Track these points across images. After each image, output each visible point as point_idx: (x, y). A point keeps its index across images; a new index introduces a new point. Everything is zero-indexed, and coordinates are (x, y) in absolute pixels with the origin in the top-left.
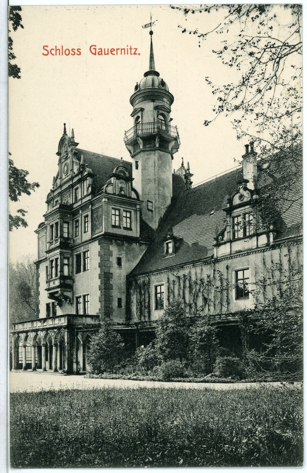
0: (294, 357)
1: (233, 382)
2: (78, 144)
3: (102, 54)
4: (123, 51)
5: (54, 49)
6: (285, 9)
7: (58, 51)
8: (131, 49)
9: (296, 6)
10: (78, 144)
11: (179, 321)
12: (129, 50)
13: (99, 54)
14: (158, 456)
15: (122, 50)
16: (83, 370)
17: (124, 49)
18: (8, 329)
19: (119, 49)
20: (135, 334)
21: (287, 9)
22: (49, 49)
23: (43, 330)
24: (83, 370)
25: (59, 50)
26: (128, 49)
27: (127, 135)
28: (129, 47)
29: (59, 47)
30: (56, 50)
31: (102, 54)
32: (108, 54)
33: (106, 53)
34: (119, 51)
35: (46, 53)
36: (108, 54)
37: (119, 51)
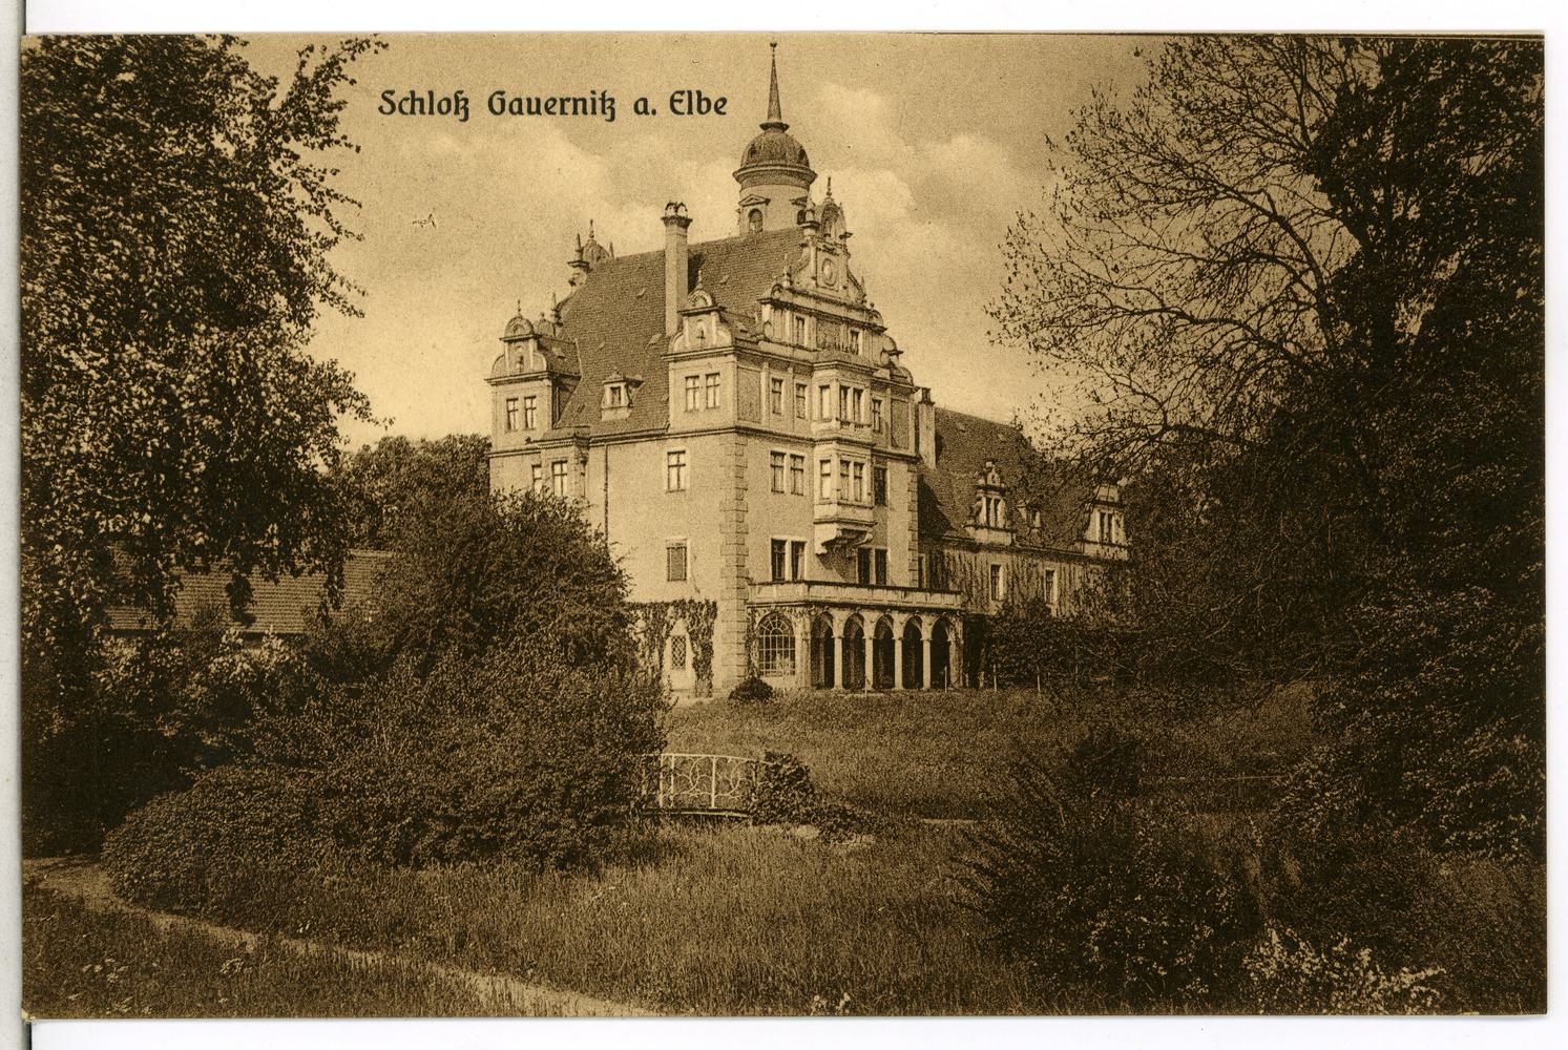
2: (787, 127)
3: (520, 112)
4: (580, 104)
5: (407, 99)
7: (417, 103)
8: (603, 100)
10: (787, 127)
11: (1054, 960)
12: (599, 104)
13: (554, 100)
15: (575, 101)
17: (584, 100)
18: (857, 524)
19: (568, 100)
20: (1463, 784)
22: (395, 99)
23: (902, 610)
25: (421, 100)
26: (594, 100)
27: (563, 313)
28: (598, 96)
29: (422, 93)
33: (534, 109)
34: (569, 107)
35: (387, 108)
36: (538, 112)
37: (569, 107)
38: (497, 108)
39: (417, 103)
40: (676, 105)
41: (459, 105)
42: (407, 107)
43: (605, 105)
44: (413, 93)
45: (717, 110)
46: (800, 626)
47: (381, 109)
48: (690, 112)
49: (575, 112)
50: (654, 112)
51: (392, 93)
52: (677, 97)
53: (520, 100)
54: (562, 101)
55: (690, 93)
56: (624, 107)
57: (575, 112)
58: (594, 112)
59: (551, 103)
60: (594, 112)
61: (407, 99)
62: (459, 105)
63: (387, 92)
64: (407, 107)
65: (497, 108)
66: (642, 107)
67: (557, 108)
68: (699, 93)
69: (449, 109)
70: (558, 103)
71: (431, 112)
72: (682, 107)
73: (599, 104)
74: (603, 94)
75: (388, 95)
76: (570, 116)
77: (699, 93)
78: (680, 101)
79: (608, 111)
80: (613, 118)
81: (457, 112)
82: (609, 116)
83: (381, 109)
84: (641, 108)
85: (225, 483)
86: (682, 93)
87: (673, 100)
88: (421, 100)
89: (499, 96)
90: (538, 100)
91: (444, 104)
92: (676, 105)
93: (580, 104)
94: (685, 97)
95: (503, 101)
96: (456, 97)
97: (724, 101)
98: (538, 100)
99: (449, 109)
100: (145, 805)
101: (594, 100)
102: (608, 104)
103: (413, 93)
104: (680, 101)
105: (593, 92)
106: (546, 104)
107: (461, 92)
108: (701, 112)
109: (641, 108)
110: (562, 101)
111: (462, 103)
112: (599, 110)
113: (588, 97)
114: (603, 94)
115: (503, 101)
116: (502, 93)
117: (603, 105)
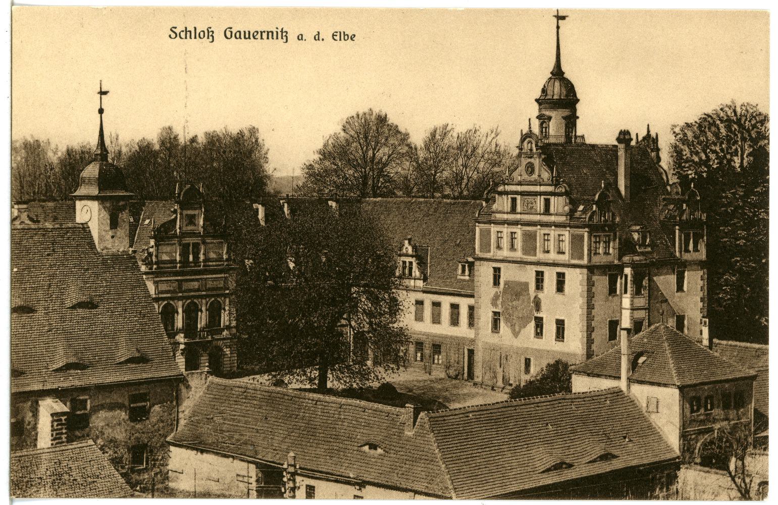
0: (692, 494)
1: (503, 381)
4: (270, 34)
5: (183, 31)
6: (24, 137)
7: (188, 33)
8: (282, 31)
9: (92, 171)
12: (280, 34)
13: (257, 32)
14: (739, 259)
16: (516, 198)
17: (272, 32)
21: (78, 143)
22: (177, 31)
24: (516, 198)
25: (190, 32)
26: (277, 32)
28: (279, 31)
30: (186, 32)
31: (240, 38)
32: (249, 38)
33: (247, 36)
34: (265, 35)
35: (173, 35)
36: (249, 38)
37: (265, 35)
38: (229, 36)
39: (188, 33)
40: (335, 37)
41: (209, 34)
42: (183, 35)
43: (283, 35)
44: (186, 28)
45: (352, 39)
46: (438, 373)
47: (170, 36)
48: (340, 40)
49: (268, 38)
50: (323, 40)
51: (175, 28)
52: (335, 34)
53: (240, 32)
54: (261, 32)
55: (340, 32)
56: (292, 37)
57: (268, 38)
58: (277, 38)
59: (255, 34)
60: (277, 38)
61: (183, 31)
62: (209, 34)
63: (173, 27)
64: (183, 35)
65: (229, 36)
66: (300, 38)
67: (259, 36)
68: (344, 33)
69: (204, 36)
70: (260, 33)
71: (195, 38)
72: (337, 38)
73: (280, 34)
74: (282, 29)
75: (174, 29)
76: (259, 40)
77: (344, 33)
78: (336, 36)
79: (285, 38)
80: (287, 42)
81: (208, 38)
82: (285, 40)
83: (170, 36)
84: (300, 38)
85: (726, 197)
86: (337, 32)
87: (333, 35)
88: (190, 32)
89: (228, 30)
90: (249, 32)
91: (202, 34)
92: (335, 37)
93: (270, 34)
94: (338, 34)
95: (231, 32)
96: (208, 30)
97: (354, 35)
98: (249, 32)
99: (204, 36)
100: (212, 375)
101: (277, 32)
102: (284, 34)
103: (186, 28)
104: (336, 36)
105: (277, 28)
106: (253, 34)
107: (210, 28)
108: (345, 40)
109: (300, 38)
110: (261, 32)
111: (211, 34)
112: (247, 33)
113: (274, 30)
114: (282, 29)
115: (231, 32)
116: (231, 28)
117: (282, 34)
